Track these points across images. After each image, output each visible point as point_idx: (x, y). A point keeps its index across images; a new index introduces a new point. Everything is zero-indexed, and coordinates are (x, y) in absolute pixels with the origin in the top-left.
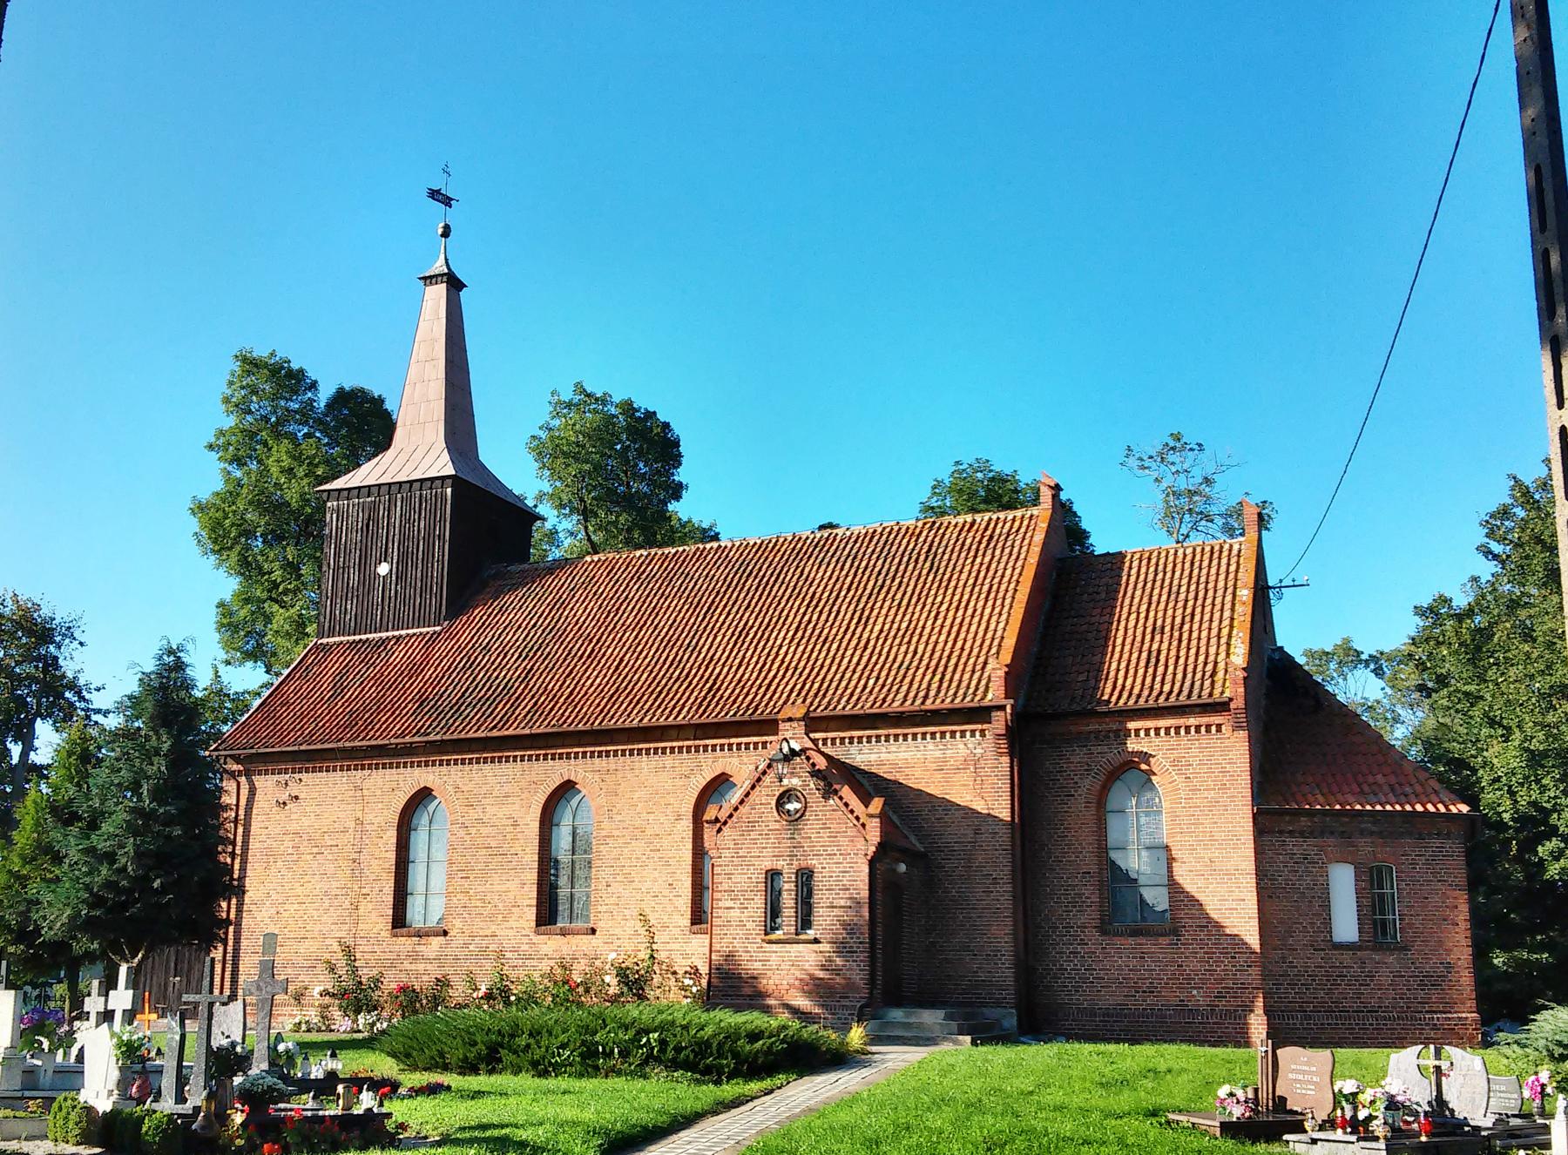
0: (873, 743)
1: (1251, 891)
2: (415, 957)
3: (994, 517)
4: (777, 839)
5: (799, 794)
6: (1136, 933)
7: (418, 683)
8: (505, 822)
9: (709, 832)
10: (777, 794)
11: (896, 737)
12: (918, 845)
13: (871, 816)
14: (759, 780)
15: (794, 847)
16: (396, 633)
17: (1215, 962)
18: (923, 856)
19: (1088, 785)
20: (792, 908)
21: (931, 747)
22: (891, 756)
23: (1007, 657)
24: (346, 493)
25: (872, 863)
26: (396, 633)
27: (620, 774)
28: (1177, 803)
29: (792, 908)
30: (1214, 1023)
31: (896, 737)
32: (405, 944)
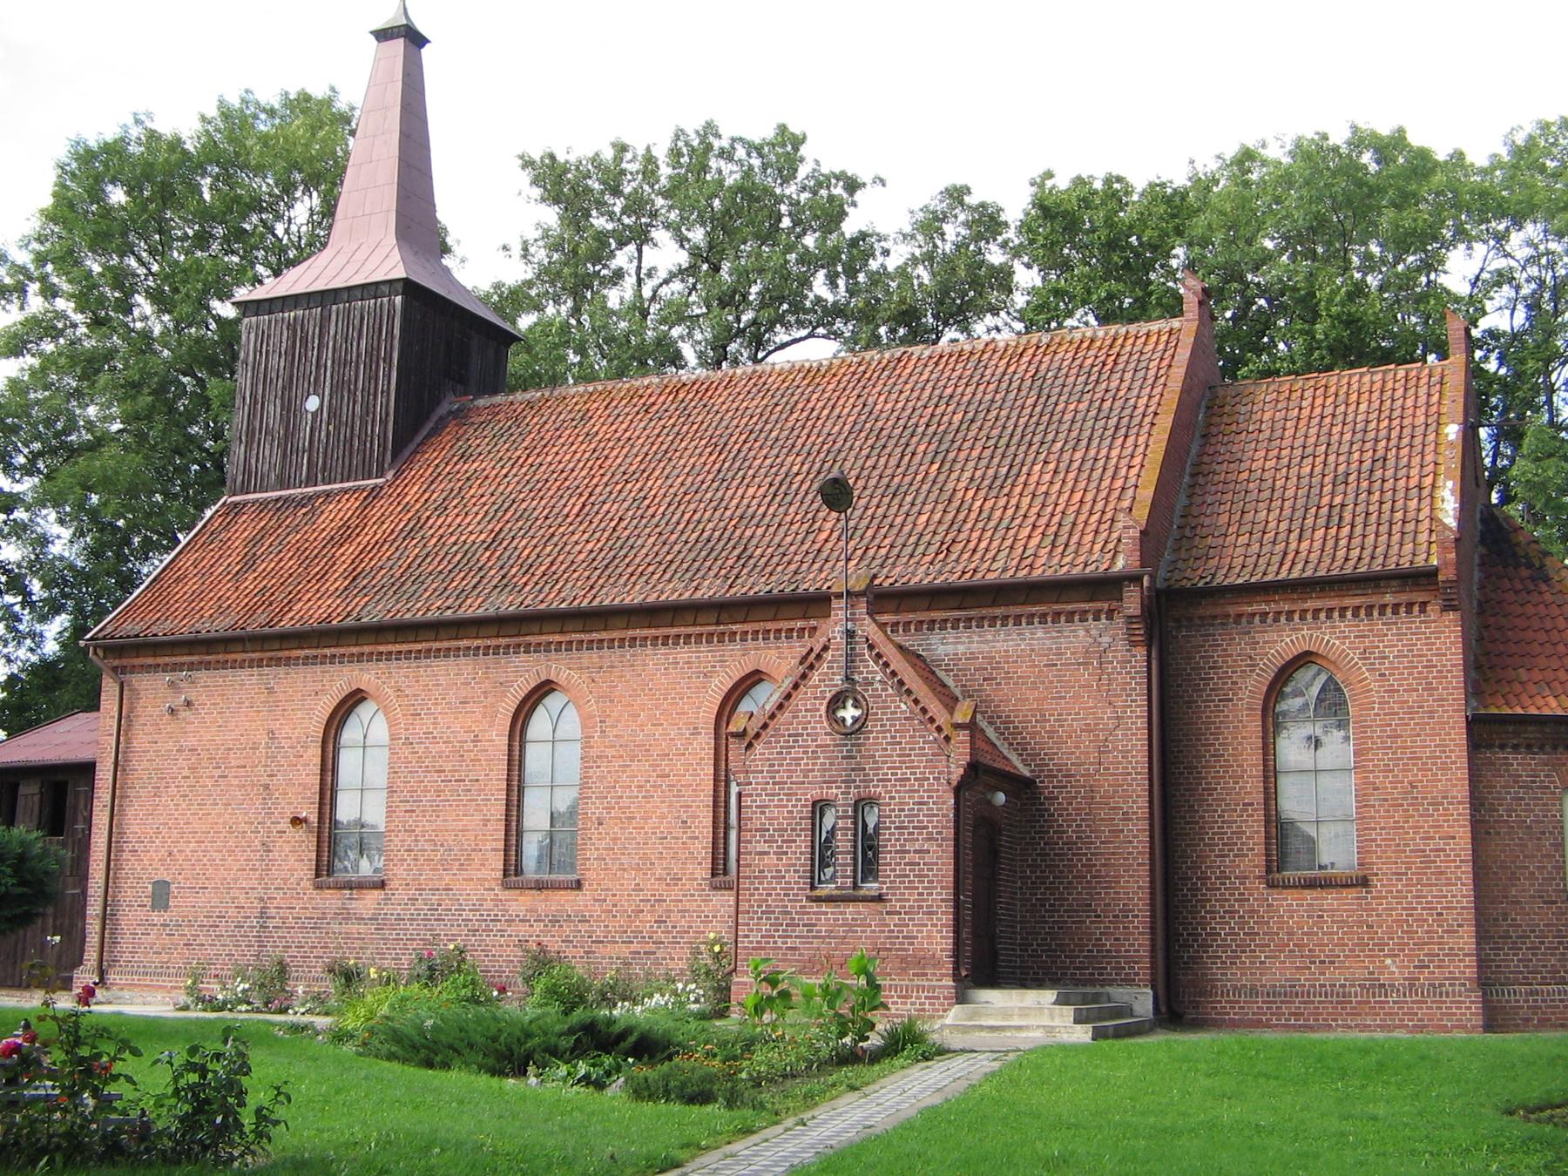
0: (1036, 624)
1: (1464, 826)
2: (345, 915)
3: (1123, 330)
4: (828, 758)
5: (859, 697)
6: (1312, 884)
7: (350, 550)
8: (465, 737)
9: (736, 748)
10: (828, 696)
11: (1043, 617)
12: (1020, 766)
13: (957, 726)
14: (804, 676)
15: (853, 770)
16: (328, 487)
17: (1416, 921)
18: (1028, 783)
19: (1252, 687)
20: (848, 853)
21: (1040, 634)
22: (985, 648)
23: (1142, 513)
24: (267, 306)
25: (957, 791)
26: (328, 487)
27: (616, 673)
28: (1368, 709)
29: (848, 853)
30: (1413, 1002)
31: (1043, 617)
32: (331, 900)
